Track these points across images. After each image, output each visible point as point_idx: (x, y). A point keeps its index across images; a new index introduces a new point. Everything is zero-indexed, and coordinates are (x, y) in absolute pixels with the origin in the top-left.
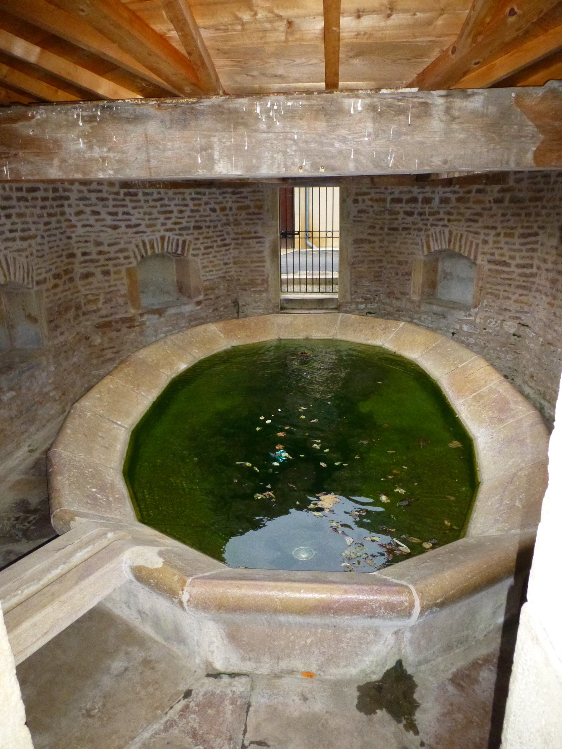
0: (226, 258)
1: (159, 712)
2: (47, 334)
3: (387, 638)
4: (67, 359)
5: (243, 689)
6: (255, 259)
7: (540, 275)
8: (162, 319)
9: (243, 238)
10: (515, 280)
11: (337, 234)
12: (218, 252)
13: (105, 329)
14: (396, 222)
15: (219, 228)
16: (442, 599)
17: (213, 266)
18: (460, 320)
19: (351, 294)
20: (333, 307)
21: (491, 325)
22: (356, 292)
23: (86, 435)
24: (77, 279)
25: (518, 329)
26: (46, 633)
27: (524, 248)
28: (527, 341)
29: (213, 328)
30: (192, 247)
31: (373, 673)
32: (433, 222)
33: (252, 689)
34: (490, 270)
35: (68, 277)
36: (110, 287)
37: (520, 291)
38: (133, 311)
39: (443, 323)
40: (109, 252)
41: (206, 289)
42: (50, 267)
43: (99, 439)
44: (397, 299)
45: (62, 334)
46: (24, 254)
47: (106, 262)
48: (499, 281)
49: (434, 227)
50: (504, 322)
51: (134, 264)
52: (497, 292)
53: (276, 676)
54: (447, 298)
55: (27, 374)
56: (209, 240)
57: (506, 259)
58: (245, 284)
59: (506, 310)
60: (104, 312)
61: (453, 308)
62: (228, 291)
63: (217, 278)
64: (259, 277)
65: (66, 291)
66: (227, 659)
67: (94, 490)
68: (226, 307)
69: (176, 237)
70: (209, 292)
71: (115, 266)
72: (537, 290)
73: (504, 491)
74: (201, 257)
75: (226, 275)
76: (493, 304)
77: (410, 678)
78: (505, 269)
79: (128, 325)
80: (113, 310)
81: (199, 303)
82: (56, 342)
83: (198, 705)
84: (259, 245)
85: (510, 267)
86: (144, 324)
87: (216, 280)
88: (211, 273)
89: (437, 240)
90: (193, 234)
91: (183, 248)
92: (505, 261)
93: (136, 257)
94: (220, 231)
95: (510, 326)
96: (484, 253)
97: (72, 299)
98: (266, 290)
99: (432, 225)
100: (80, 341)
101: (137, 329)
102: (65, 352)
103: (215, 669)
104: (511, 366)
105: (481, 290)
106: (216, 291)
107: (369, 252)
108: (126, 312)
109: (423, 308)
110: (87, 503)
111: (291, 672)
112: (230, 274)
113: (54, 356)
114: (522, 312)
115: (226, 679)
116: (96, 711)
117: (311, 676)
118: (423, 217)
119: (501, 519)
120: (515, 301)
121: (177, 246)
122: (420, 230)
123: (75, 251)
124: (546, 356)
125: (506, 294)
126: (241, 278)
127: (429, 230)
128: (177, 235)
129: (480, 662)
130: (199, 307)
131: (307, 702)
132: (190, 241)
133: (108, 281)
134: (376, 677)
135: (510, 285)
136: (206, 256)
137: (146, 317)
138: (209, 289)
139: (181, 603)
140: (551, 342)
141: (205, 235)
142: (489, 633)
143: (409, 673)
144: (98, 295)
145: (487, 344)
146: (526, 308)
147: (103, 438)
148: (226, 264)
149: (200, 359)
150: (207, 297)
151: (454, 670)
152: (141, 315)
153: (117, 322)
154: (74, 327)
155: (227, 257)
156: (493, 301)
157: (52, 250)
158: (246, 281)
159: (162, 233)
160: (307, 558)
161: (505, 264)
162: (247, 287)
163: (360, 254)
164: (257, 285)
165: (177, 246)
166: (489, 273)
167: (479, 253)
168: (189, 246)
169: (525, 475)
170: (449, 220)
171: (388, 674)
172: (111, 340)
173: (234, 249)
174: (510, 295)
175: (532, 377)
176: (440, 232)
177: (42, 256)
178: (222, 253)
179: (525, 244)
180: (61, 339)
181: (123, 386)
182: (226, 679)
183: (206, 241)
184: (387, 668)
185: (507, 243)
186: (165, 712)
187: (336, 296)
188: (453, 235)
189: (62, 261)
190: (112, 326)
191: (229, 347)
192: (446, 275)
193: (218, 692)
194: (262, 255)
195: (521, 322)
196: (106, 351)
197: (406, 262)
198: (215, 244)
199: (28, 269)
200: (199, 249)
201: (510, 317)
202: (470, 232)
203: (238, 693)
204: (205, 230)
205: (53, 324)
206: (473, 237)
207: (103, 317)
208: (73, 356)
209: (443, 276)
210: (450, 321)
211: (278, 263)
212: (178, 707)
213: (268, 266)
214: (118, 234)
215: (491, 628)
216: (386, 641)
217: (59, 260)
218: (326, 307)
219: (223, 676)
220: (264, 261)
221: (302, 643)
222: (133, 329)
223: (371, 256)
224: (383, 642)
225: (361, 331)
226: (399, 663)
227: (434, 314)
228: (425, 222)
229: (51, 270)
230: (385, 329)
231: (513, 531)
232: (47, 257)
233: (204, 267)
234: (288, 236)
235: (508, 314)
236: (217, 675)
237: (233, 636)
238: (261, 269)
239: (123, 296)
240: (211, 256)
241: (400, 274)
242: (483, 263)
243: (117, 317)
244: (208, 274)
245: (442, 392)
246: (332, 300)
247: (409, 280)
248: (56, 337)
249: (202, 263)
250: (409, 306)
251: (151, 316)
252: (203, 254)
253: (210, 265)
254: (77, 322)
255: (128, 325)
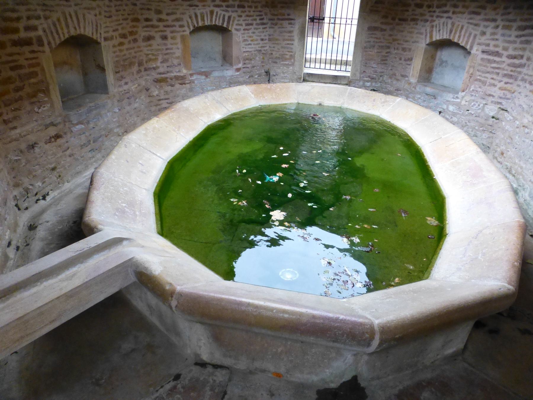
0: (263, 35)
1: (152, 389)
2: (113, 83)
3: (347, 357)
4: (130, 104)
5: (221, 379)
6: (286, 38)
7: (529, 66)
8: (208, 80)
9: (278, 19)
10: (503, 69)
11: (355, 22)
12: (257, 29)
13: (162, 84)
14: (407, 13)
15: (259, 9)
16: (400, 335)
17: (252, 41)
18: (448, 101)
19: (361, 73)
20: (345, 83)
21: (474, 108)
22: (364, 72)
23: (128, 162)
24: (140, 40)
25: (498, 112)
26: (53, 321)
27: (519, 40)
28: (504, 123)
29: (246, 89)
30: (236, 22)
31: (332, 382)
32: (439, 14)
33: (230, 380)
34: (482, 59)
35: (133, 37)
36: (167, 49)
37: (506, 80)
38: (185, 71)
39: (433, 102)
40: (167, 20)
41: (245, 59)
42: (117, 27)
43: (139, 165)
44: (398, 80)
45: (126, 83)
46: (93, 12)
47: (165, 29)
48: (489, 69)
49: (439, 19)
50: (486, 106)
51: (188, 32)
52: (485, 79)
53: (251, 372)
54: (440, 82)
55: (94, 112)
56: (250, 18)
57: (499, 49)
58: (276, 58)
59: (490, 95)
60: (161, 70)
61: (443, 91)
62: (262, 62)
63: (254, 51)
64: (287, 53)
65: (131, 49)
66: (212, 353)
67: (124, 205)
68: (260, 75)
69: (223, 13)
70: (247, 61)
71: (172, 32)
72: (523, 80)
73: (469, 245)
74: (242, 32)
75: (263, 49)
76: (479, 90)
77: (363, 389)
78: (497, 59)
79: (180, 82)
80: (169, 69)
81: (238, 70)
82: (121, 89)
83: (183, 387)
84: (290, 26)
85: (501, 57)
86: (194, 82)
87: (253, 53)
88: (250, 46)
89: (439, 31)
90: (237, 11)
91: (228, 22)
92: (497, 52)
93: (189, 27)
94: (260, 11)
95: (491, 110)
96: (479, 44)
97: (136, 57)
98: (293, 64)
99: (438, 17)
100: (141, 91)
101: (188, 86)
102: (128, 98)
103: (202, 360)
104: (485, 143)
105: (471, 77)
106: (253, 62)
107: (380, 38)
108: (179, 71)
109: (418, 89)
110: (115, 214)
111: (264, 371)
112: (265, 48)
113: (118, 101)
114: (504, 98)
115: (210, 369)
116: (103, 381)
117: (280, 376)
118: (431, 9)
119: (463, 268)
120: (500, 88)
121: (224, 19)
122: (427, 21)
123: (140, 17)
124: (519, 137)
125: (492, 81)
126: (274, 53)
127: (434, 21)
128: (223, 11)
129: (424, 384)
130: (238, 73)
131: (273, 397)
132: (234, 17)
133: (165, 44)
134: (333, 386)
135: (498, 74)
136: (246, 31)
137: (195, 77)
138: (247, 59)
139: (171, 308)
140: (526, 125)
141: (247, 13)
142: (435, 361)
143: (362, 386)
144: (158, 55)
145: (468, 124)
146: (509, 96)
147: (142, 165)
148: (262, 40)
149: (232, 112)
150: (245, 66)
151: (401, 387)
152: (191, 75)
153: (171, 79)
154: (136, 79)
155: (265, 33)
156: (480, 87)
157: (119, 13)
158: (278, 55)
159: (212, 8)
160: (291, 279)
161: (497, 54)
162: (278, 61)
163: (372, 40)
164: (286, 59)
165: (224, 19)
166: (481, 63)
167: (476, 43)
168: (233, 21)
169: (490, 233)
170: (454, 13)
171: (344, 384)
172: (166, 93)
173: (270, 28)
174: (496, 83)
175: (502, 154)
176: (444, 23)
177: (110, 17)
178: (259, 30)
179: (521, 36)
180: (126, 87)
181: (167, 127)
182: (210, 369)
183: (247, 18)
184: (344, 380)
185: (503, 35)
186: (157, 389)
187: (348, 74)
188: (456, 25)
189: (128, 24)
190: (167, 82)
191: (257, 105)
192: (442, 62)
193: (202, 379)
194: (292, 35)
195: (502, 107)
196: (162, 102)
197: (410, 50)
198: (255, 22)
199: (97, 26)
200: (241, 25)
201: (492, 102)
202: (471, 24)
203: (218, 382)
204: (247, 9)
205: (118, 75)
206: (473, 29)
207: (160, 74)
208: (135, 103)
209: (439, 63)
210: (439, 102)
211: (304, 44)
212: (168, 387)
213: (296, 42)
214: (176, 5)
215: (438, 357)
216: (345, 360)
217: (125, 22)
218: (339, 82)
219: (209, 365)
220: (293, 40)
221: (274, 350)
222: (184, 85)
223: (381, 42)
224: (342, 360)
225: (365, 102)
226: (355, 378)
227: (427, 94)
228: (432, 14)
229: (117, 30)
230: (384, 102)
231: (473, 281)
232: (114, 18)
233: (245, 40)
234: (315, 21)
235: (491, 99)
236: (203, 365)
237: (217, 338)
238: (290, 46)
239: (178, 58)
240: (250, 31)
241: (403, 59)
242: (477, 52)
243: (172, 74)
244: (247, 47)
245: (424, 156)
246: (345, 77)
247: (409, 65)
248: (120, 86)
249: (243, 37)
250: (407, 86)
251: (199, 77)
252: (244, 30)
253: (250, 39)
254: (139, 75)
255: (180, 82)
